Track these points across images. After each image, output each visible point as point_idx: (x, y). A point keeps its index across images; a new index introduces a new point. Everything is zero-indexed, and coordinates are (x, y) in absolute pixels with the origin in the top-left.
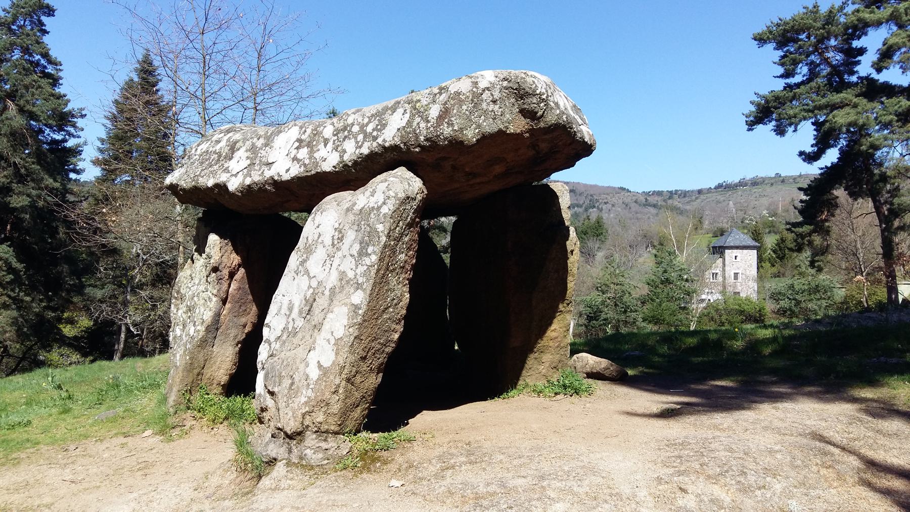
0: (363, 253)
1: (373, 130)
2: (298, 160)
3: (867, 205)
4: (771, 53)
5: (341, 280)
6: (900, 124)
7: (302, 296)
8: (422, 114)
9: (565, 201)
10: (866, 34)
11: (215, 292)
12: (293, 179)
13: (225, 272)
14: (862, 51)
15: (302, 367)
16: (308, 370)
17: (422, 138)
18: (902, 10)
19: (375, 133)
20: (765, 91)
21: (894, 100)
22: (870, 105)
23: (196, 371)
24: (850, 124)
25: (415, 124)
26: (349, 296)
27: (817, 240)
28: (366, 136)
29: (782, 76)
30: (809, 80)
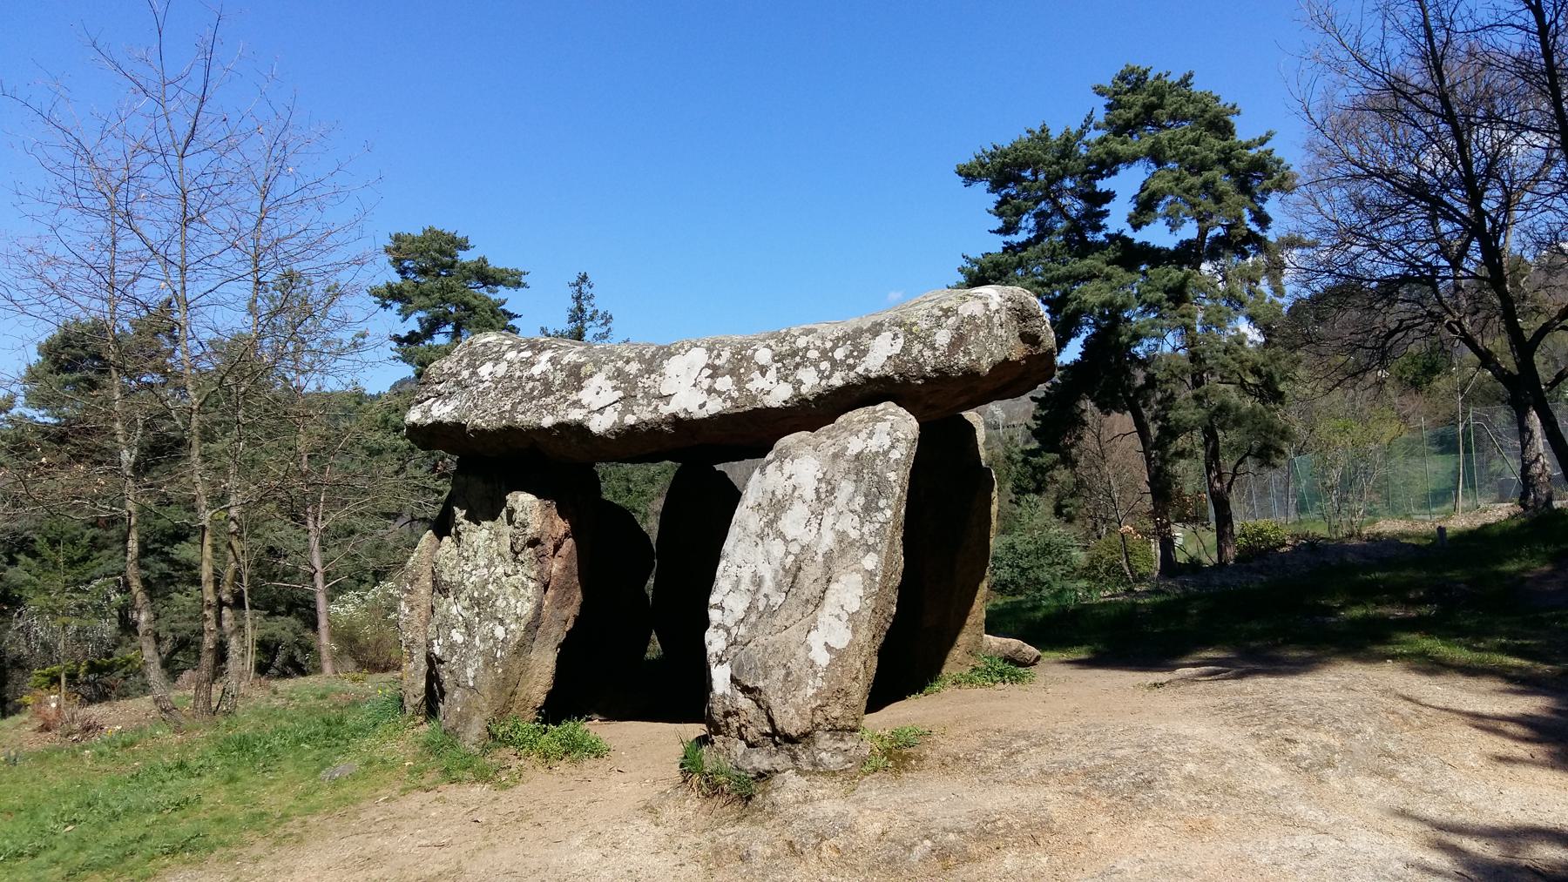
0: (869, 508)
1: (847, 357)
2: (720, 394)
3: (1122, 422)
4: (983, 197)
5: (840, 542)
6: (1172, 304)
7: (776, 564)
8: (927, 341)
9: (981, 435)
10: (1115, 173)
11: (533, 574)
12: (711, 417)
13: (550, 546)
14: (1108, 196)
15: (801, 652)
16: (812, 655)
17: (929, 369)
18: (1165, 142)
19: (851, 361)
20: (976, 254)
21: (1161, 270)
22: (1128, 277)
23: (509, 690)
24: (1103, 305)
25: (915, 352)
26: (858, 561)
27: (1062, 475)
28: (835, 364)
29: (999, 231)
30: (1038, 239)
